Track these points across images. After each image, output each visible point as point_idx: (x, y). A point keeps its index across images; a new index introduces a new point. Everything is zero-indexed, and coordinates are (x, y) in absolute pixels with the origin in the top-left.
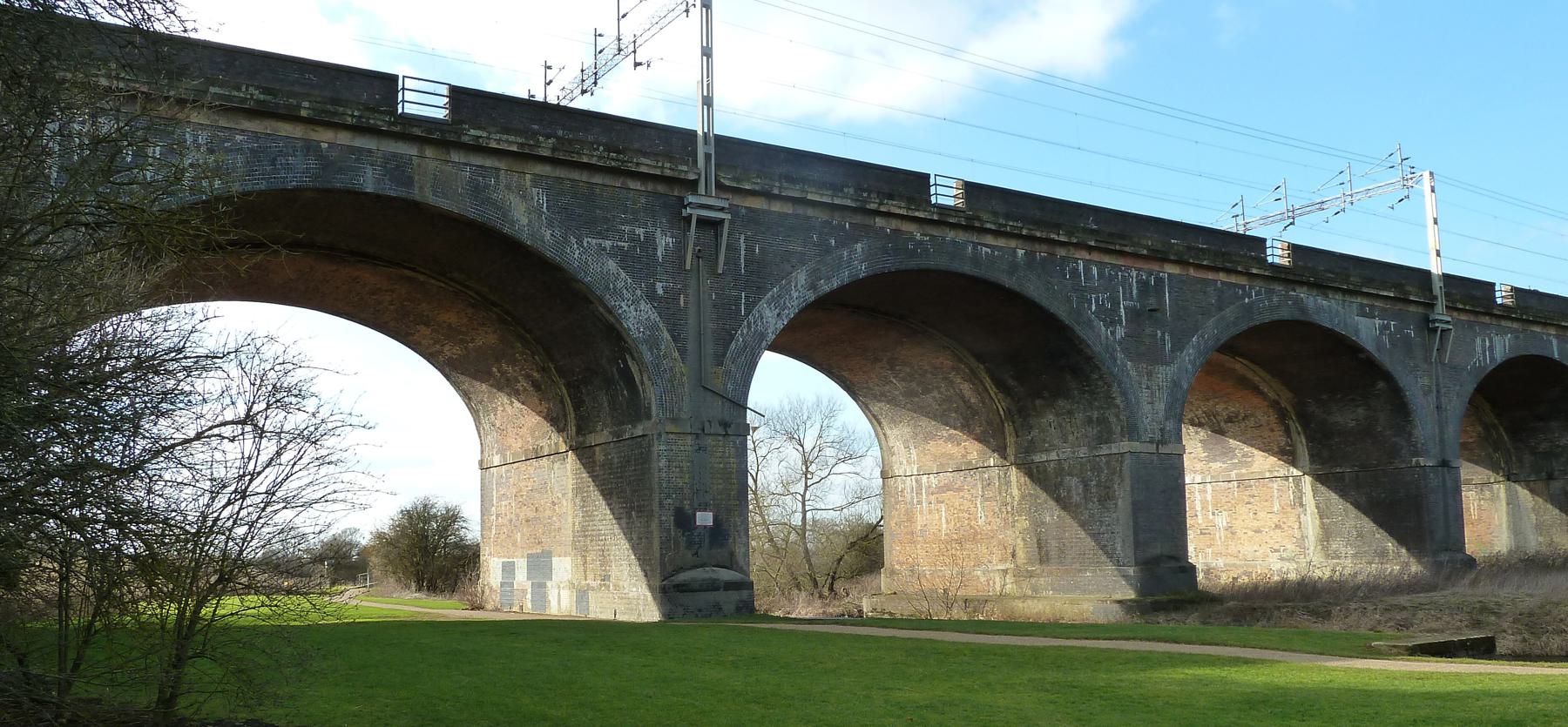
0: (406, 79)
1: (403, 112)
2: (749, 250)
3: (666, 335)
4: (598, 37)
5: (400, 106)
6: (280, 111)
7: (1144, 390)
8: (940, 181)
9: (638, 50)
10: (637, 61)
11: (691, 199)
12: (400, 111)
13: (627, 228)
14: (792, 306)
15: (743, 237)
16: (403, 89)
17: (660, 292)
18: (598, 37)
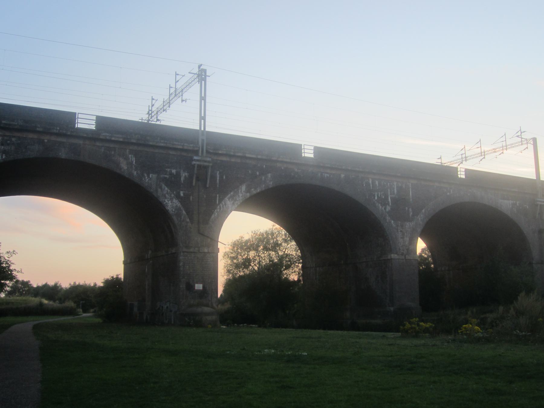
0: (79, 114)
1: (304, 156)
2: (221, 177)
3: (184, 212)
4: (177, 76)
5: (76, 125)
6: (38, 129)
7: (399, 233)
8: (306, 147)
9: (183, 95)
10: (183, 99)
11: (195, 158)
12: (76, 126)
13: (168, 170)
14: (239, 200)
15: (218, 172)
16: (78, 118)
17: (182, 195)
18: (177, 76)
